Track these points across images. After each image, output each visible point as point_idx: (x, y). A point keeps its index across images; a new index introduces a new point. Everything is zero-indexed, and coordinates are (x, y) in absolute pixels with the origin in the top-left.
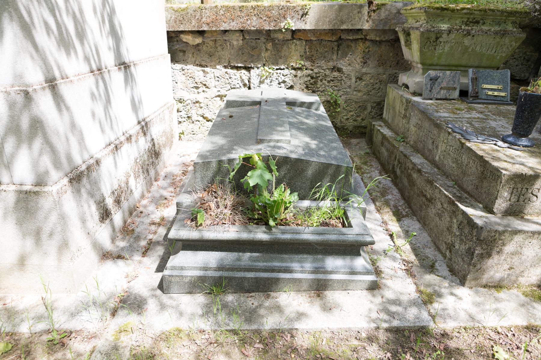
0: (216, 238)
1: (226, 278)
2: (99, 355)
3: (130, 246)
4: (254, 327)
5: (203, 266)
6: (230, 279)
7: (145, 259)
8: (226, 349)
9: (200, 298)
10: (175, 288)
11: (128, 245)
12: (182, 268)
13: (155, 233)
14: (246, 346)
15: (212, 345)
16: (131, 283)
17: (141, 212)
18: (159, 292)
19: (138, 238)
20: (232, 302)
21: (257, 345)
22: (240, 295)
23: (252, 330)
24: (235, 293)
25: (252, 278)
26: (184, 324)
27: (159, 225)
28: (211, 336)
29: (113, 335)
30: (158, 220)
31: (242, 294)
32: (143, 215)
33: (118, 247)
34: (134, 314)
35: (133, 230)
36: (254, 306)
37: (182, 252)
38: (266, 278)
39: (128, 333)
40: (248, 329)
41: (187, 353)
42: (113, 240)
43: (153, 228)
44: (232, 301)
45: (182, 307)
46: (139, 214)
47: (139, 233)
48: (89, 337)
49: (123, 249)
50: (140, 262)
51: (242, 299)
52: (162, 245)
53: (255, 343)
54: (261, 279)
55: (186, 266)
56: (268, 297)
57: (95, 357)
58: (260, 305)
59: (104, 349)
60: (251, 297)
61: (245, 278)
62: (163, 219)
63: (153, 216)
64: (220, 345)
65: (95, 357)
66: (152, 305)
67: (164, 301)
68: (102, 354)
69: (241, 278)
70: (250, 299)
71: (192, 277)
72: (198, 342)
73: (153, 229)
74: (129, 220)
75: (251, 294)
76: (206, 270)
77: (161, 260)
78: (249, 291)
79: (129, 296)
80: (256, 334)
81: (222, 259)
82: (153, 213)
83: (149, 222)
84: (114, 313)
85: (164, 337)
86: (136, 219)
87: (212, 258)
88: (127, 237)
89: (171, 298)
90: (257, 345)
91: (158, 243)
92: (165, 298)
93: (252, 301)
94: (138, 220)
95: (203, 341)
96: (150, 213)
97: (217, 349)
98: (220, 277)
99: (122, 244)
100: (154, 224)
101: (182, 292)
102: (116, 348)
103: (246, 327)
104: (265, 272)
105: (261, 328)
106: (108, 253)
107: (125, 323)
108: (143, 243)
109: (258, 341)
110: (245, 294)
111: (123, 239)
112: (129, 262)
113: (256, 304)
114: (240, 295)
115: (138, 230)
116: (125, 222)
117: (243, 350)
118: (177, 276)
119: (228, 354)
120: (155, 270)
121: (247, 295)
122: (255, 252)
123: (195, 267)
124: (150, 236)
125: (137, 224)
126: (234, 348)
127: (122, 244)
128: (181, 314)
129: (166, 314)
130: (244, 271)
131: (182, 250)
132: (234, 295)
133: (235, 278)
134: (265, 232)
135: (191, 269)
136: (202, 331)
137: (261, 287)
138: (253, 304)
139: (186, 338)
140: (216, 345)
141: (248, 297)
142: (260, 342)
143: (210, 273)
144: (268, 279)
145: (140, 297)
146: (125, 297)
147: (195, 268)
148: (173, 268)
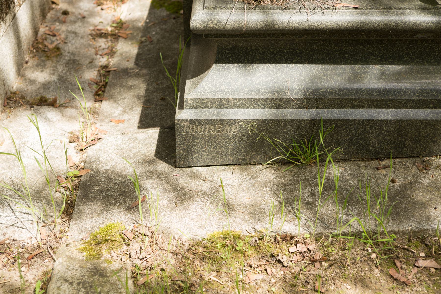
0: (306, 25)
1: (328, 123)
2: (65, 286)
3: (62, 80)
4: (409, 226)
5: (270, 96)
6: (339, 125)
7: (106, 106)
8: (351, 271)
9: (266, 174)
10: (203, 153)
11: (54, 78)
12: (222, 104)
13: (111, 53)
14: (398, 264)
15: (317, 265)
16: (91, 152)
17: (65, 13)
18: (162, 166)
19: (74, 65)
20: (342, 179)
21: (422, 263)
22: (359, 166)
23: (404, 233)
24: (345, 161)
25: (388, 122)
26: (241, 226)
27: (115, 37)
28: (311, 247)
29: (83, 250)
30: (110, 29)
31: (362, 164)
32: (70, 18)
33: (32, 82)
34: (117, 210)
35: (57, 48)
36: (397, 186)
37: (214, 65)
38: (421, 122)
39: (117, 244)
40: (396, 230)
41: (264, 281)
42: (20, 66)
43: (102, 43)
44: (342, 176)
45: (229, 192)
46: (62, 17)
47: (73, 54)
48: (26, 255)
49: (46, 86)
50: (94, 112)
51: (366, 173)
52: (137, 75)
53: (417, 258)
54: (411, 123)
55: (230, 97)
56: (426, 167)
57: (59, 288)
58: (411, 183)
59: (76, 273)
60: (385, 167)
61: (373, 123)
62: (120, 25)
63: (95, 20)
64: (340, 263)
65: (59, 288)
66: (155, 193)
67: (181, 181)
68: (71, 284)
69: (362, 123)
70: (383, 172)
71: (247, 122)
72: (284, 259)
73: (103, 46)
74: (42, 30)
75: (383, 163)
76: (278, 107)
77: (144, 103)
78: (378, 156)
79: (92, 176)
80: (414, 241)
81: (314, 79)
82: (92, 14)
83: (89, 32)
84: (69, 212)
85: (204, 252)
86: (57, 26)
87: (293, 77)
88: (49, 63)
89: (194, 176)
90: (422, 263)
91: (125, 73)
92: (181, 177)
93: (391, 175)
94: (62, 29)
95: (295, 258)
96: (85, 14)
97: (331, 273)
98: (314, 124)
99: (41, 76)
100: (101, 35)
101: (219, 161)
102: (99, 272)
103: (392, 226)
104: (418, 108)
105: (426, 227)
106: (15, 93)
107: (103, 226)
108: (91, 75)
109: (422, 255)
110: (369, 163)
111: (41, 66)
112: (70, 111)
113: (400, 181)
114: (359, 166)
115: (70, 48)
116: (36, 31)
117: (392, 272)
118: (209, 122)
119: (361, 282)
120: (136, 124)
121: (374, 164)
122: (391, 63)
123: (251, 100)
124: (103, 61)
125: (63, 36)
126: (371, 270)
127: (41, 76)
128: (229, 207)
129: (196, 206)
130: (369, 107)
131: (219, 61)
132: (344, 165)
133: (347, 123)
134: (423, 9)
135: (242, 106)
136: (288, 239)
137: (409, 143)
138: (393, 181)
139: (250, 252)
140: (325, 264)
141: (377, 169)
142: (427, 257)
143: (290, 114)
144: (426, 123)
145: (120, 176)
146: (83, 179)
147: (252, 103)
148: (201, 104)
